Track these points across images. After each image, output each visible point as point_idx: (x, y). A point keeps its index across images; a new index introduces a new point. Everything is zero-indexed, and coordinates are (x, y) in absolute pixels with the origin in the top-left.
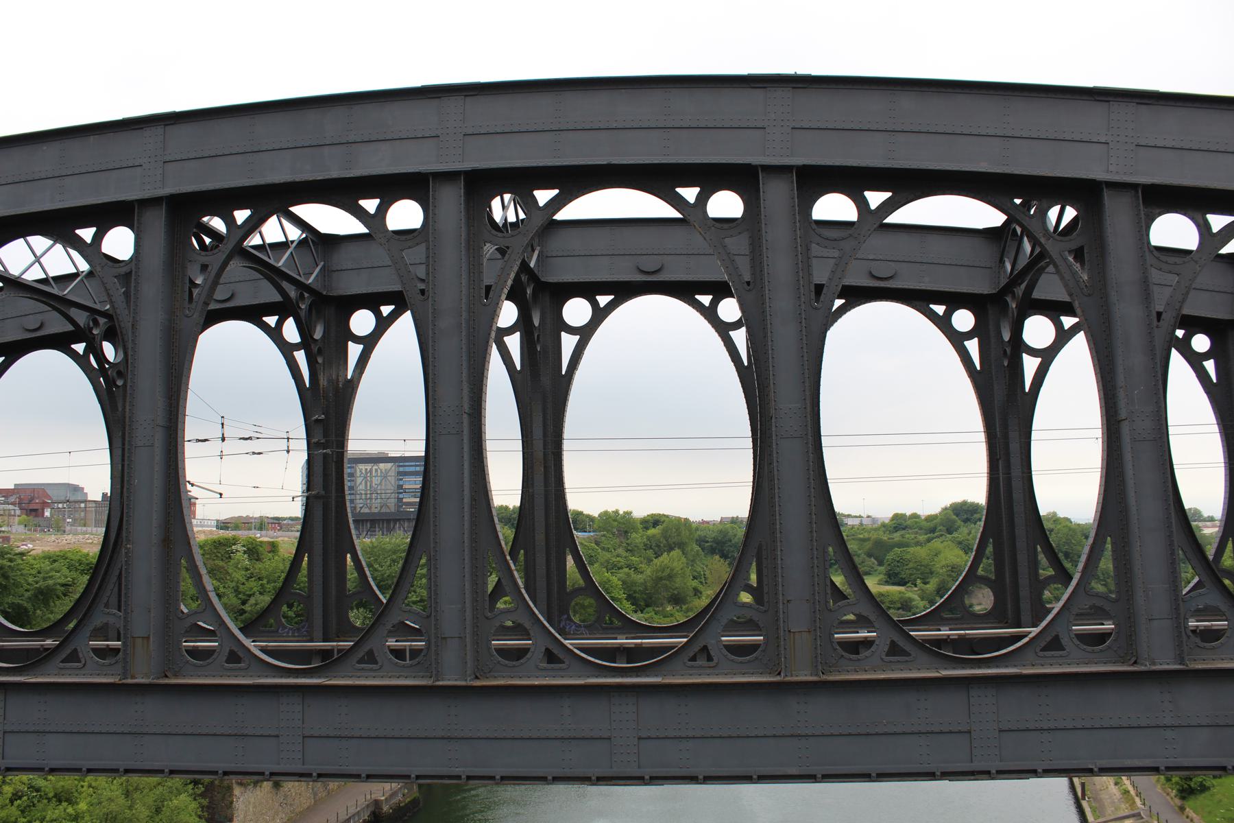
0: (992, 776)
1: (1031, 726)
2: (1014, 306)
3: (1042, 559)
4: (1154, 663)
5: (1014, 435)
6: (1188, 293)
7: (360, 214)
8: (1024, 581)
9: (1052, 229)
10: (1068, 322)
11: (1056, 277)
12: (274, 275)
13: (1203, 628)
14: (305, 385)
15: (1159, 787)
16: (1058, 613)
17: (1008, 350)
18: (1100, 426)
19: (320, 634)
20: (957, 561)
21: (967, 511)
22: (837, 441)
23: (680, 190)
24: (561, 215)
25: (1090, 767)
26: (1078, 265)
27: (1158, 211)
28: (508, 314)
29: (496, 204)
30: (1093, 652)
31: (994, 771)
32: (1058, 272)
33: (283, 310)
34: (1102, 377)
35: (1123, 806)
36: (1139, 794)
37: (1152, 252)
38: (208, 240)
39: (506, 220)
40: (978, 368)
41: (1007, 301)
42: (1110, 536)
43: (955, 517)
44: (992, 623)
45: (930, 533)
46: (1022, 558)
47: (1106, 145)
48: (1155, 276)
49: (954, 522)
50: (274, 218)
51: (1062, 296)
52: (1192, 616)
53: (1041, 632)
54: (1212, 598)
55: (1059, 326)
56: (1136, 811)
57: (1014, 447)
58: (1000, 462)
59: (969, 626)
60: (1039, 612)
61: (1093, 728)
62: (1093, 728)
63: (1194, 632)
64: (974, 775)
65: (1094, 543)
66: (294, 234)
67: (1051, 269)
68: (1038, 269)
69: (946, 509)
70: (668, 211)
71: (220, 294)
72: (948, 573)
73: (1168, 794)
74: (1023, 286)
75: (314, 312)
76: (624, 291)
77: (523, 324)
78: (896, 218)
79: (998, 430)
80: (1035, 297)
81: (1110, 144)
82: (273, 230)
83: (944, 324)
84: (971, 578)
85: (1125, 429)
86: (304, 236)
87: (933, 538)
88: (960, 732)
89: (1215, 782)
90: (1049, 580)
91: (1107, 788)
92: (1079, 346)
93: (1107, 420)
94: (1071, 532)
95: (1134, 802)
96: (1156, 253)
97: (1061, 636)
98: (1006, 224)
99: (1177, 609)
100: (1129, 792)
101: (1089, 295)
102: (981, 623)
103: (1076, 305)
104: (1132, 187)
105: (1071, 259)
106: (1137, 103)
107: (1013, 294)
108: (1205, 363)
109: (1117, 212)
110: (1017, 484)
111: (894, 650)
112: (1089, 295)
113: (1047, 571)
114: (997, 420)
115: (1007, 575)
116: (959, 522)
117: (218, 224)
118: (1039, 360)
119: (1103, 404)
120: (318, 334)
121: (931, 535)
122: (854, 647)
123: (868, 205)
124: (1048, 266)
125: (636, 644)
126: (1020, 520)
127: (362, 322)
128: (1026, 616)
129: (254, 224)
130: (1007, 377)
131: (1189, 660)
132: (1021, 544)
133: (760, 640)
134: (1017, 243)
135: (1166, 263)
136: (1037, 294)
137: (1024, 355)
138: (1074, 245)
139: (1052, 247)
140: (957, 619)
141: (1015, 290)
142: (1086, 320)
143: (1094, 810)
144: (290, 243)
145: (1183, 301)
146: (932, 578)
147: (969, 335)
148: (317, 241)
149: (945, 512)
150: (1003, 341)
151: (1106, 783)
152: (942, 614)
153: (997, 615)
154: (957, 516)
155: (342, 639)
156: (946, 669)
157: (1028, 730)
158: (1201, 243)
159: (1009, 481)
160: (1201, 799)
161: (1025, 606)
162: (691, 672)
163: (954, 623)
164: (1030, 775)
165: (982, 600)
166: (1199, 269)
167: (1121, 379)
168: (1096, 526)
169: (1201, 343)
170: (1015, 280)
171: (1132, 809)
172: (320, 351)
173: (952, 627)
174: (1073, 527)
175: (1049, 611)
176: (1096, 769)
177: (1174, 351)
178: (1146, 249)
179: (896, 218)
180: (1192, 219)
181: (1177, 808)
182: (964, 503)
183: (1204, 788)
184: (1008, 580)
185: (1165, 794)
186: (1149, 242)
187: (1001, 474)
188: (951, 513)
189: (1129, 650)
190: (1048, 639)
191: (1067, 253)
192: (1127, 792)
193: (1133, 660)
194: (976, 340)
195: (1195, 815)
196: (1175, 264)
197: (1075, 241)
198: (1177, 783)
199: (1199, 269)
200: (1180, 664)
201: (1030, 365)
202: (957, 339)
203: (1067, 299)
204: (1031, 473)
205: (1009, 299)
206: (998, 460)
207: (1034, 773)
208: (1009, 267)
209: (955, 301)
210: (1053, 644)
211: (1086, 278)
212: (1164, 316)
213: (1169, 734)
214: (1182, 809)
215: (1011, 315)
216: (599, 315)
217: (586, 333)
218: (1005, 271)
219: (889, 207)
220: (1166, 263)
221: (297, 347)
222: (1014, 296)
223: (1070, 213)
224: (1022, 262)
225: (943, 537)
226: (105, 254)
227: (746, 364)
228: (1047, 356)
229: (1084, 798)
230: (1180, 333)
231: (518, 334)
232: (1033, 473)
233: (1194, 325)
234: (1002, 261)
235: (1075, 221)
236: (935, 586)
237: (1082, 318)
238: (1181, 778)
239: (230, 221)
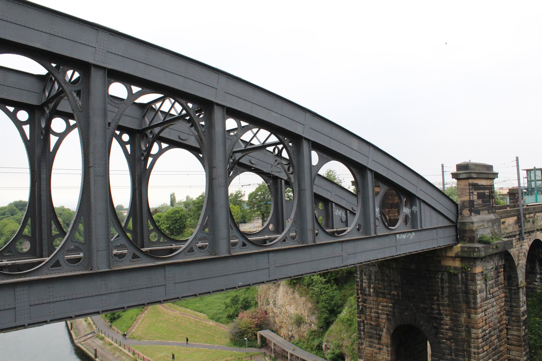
0: (26, 327)
1: (45, 301)
2: (48, 112)
3: (54, 227)
4: (99, 269)
5: (44, 171)
6: (121, 116)
8: (45, 236)
9: (68, 81)
10: (72, 122)
11: (67, 102)
13: (119, 253)
15: (102, 319)
16: (59, 250)
17: (44, 132)
18: (81, 169)
19: (331, 227)
20: (15, 228)
21: (21, 205)
25: (71, 316)
26: (78, 98)
27: (113, 80)
30: (74, 266)
31: (126, 307)
32: (68, 100)
34: (84, 148)
35: (88, 330)
36: (94, 324)
37: (109, 97)
40: (29, 139)
41: (45, 109)
42: (83, 216)
43: (15, 208)
44: (29, 256)
45: (2, 215)
46: (44, 226)
47: (95, 49)
48: (109, 107)
49: (15, 210)
51: (69, 110)
52: (115, 249)
53: (51, 259)
54: (123, 241)
55: (68, 124)
56: (93, 331)
57: (43, 176)
58: (36, 183)
59: (18, 259)
60: (52, 248)
61: (73, 299)
62: (73, 299)
63: (115, 255)
64: (17, 328)
65: (76, 219)
67: (66, 98)
68: (60, 97)
69: (11, 204)
72: (11, 234)
73: (106, 322)
74: (53, 104)
79: (36, 168)
80: (59, 109)
81: (97, 48)
83: (13, 116)
84: (20, 235)
85: (92, 170)
87: (3, 218)
88: (10, 309)
89: (123, 314)
90: (57, 236)
91: (82, 323)
92: (75, 134)
93: (85, 167)
94: (70, 215)
95: (93, 327)
96: (110, 98)
97: (60, 260)
98: (47, 74)
99: (109, 246)
100: (90, 323)
101: (81, 112)
102: (23, 257)
103: (75, 115)
104: (104, 68)
105: (75, 95)
106: (110, 34)
107: (48, 106)
108: (126, 146)
109: (97, 77)
110: (44, 193)
111: (135, 256)
112: (81, 112)
113: (55, 232)
114: (36, 164)
115: (37, 234)
116: (17, 210)
118: (58, 138)
119: (83, 160)
121: (3, 216)
122: (121, 256)
124: (65, 96)
125: (12, 263)
126: (44, 209)
128: (45, 253)
130: (42, 144)
131: (112, 266)
132: (44, 220)
133: (82, 256)
134: (52, 84)
135: (114, 102)
136: (59, 108)
137: (51, 135)
138: (77, 89)
139: (67, 88)
140: (11, 256)
141: (49, 105)
142: (79, 122)
143: (76, 333)
145: (119, 120)
146: (2, 237)
147: (25, 123)
149: (11, 205)
150: (41, 127)
151: (81, 322)
152: (4, 254)
153: (32, 253)
154: (17, 208)
155: (232, 238)
156: (3, 280)
157: (43, 303)
158: (128, 97)
160: (118, 322)
161: (45, 248)
162: (51, 273)
163: (9, 258)
164: (44, 324)
165: (26, 246)
166: (126, 107)
167: (91, 149)
168: (77, 212)
169: (126, 137)
170: (49, 100)
171: (91, 330)
173: (9, 259)
174: (71, 212)
175: (56, 249)
176: (73, 316)
177: (114, 139)
178: (107, 96)
180: (126, 86)
181: (109, 326)
182: (21, 201)
183: (119, 317)
184: (37, 237)
185: (105, 322)
186: (108, 93)
187: (36, 188)
188: (14, 206)
189: (89, 264)
190: (54, 262)
191: (73, 92)
192: (90, 324)
193: (302, 243)
194: (28, 125)
195: (115, 328)
196: (118, 104)
197: (77, 87)
198: (109, 317)
199: (126, 107)
200: (109, 268)
201: (53, 140)
202: (19, 124)
203: (72, 112)
204: (50, 188)
205: (46, 109)
206: (35, 182)
207: (46, 322)
208: (47, 94)
209: (19, 106)
210: (57, 264)
211: (80, 104)
212: (111, 124)
213: (104, 297)
214: (111, 326)
215: (46, 115)
218: (45, 96)
220: (114, 102)
222: (48, 108)
223: (77, 75)
224: (54, 93)
225: (9, 217)
226: (112, 96)
228: (62, 136)
229: (72, 329)
230: (118, 132)
232: (52, 188)
233: (124, 129)
234: (44, 91)
235: (78, 79)
236: (4, 240)
237: (77, 121)
238: (111, 314)
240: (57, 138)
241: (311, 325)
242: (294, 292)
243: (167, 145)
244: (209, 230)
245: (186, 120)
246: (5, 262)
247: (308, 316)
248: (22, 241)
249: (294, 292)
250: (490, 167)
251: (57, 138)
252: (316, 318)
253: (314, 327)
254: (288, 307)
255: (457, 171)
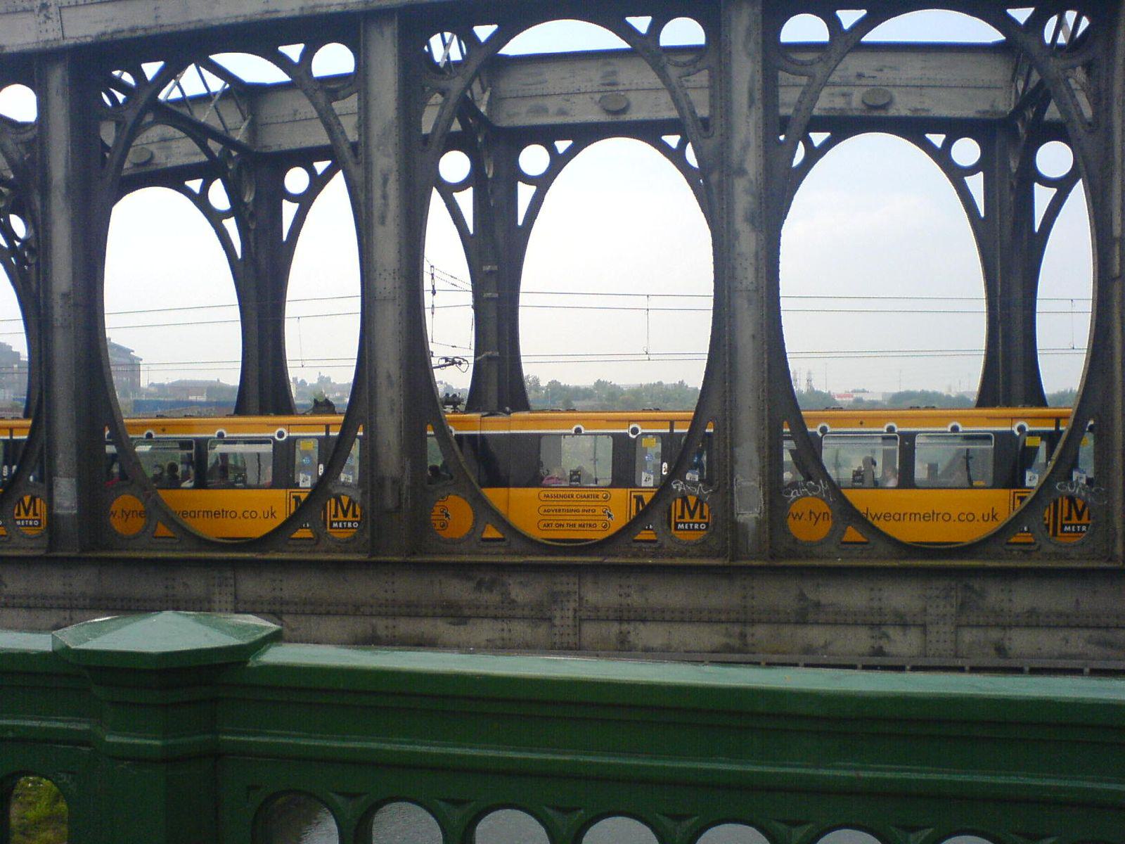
7: (282, 62)
12: (199, 133)
14: (236, 256)
22: (696, 303)
23: (630, 20)
24: (505, 51)
28: (454, 166)
29: (435, 42)
33: (207, 173)
38: (121, 97)
39: (448, 57)
50: (193, 65)
66: (216, 84)
70: (618, 43)
71: (132, 158)
75: (244, 172)
76: (585, 135)
77: (475, 179)
78: (872, 36)
82: (192, 82)
83: (942, 157)
86: (228, 86)
117: (128, 78)
118: (1055, 190)
120: (249, 198)
123: (840, 24)
127: (296, 180)
129: (171, 73)
144: (212, 96)
148: (240, 91)
159: (1007, 337)
172: (252, 215)
179: (872, 36)
202: (957, 175)
209: (955, 129)
216: (558, 163)
217: (543, 183)
219: (865, 25)
221: (227, 215)
227: (520, 222)
231: (470, 190)
239: (139, 75)
240: (533, 189)
243: (569, 143)
245: (466, 92)
246: (5, 722)
251: (533, 189)
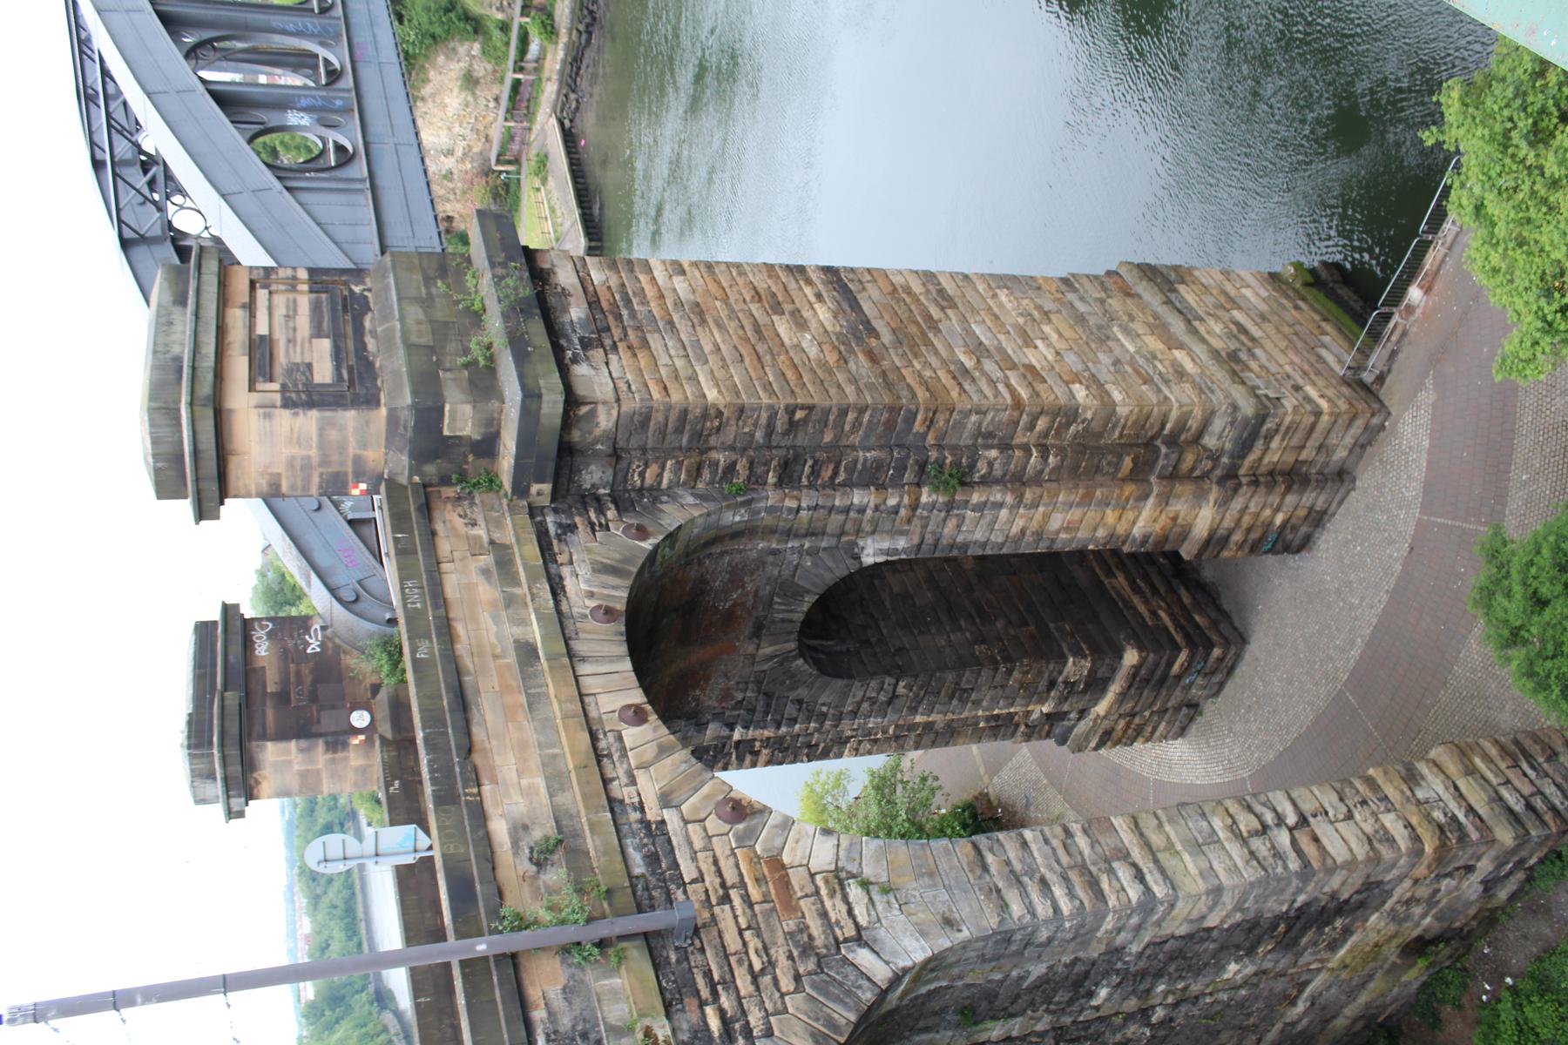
241: (474, 56)
242: (423, 99)
244: (1141, 647)
247: (459, 61)
248: (1063, 536)
249: (423, 99)
250: (204, 631)
252: (462, 45)
253: (476, 48)
254: (450, 111)
255: (186, 498)
